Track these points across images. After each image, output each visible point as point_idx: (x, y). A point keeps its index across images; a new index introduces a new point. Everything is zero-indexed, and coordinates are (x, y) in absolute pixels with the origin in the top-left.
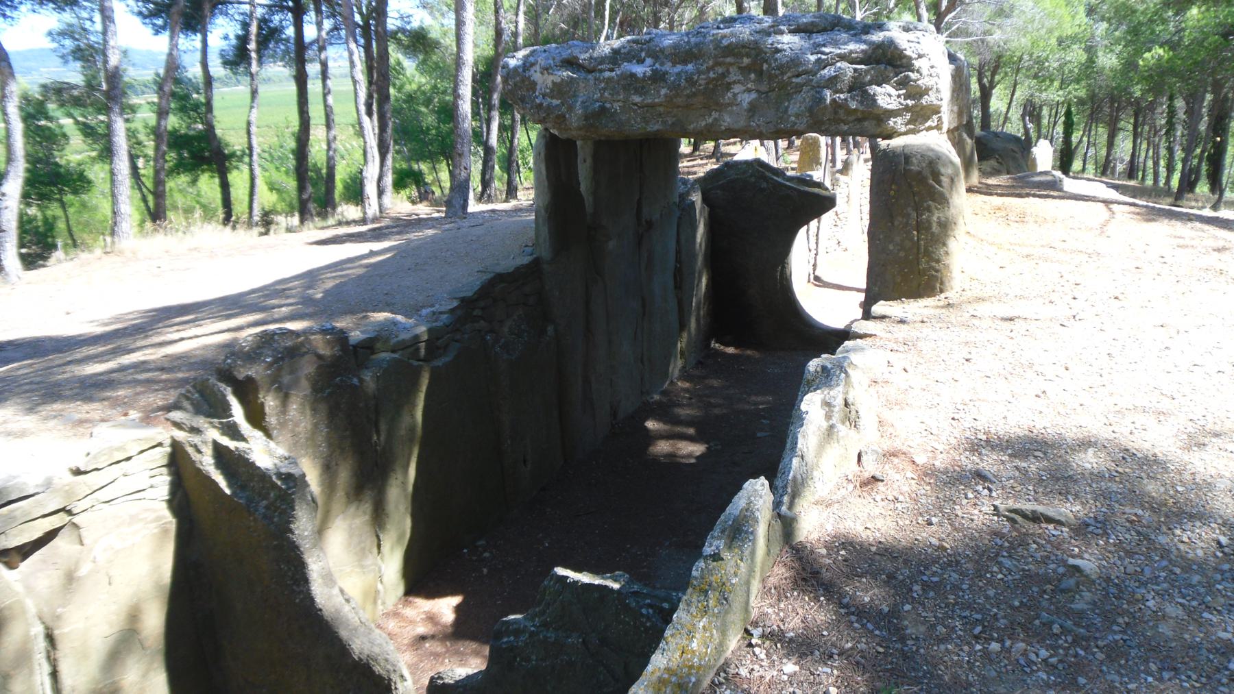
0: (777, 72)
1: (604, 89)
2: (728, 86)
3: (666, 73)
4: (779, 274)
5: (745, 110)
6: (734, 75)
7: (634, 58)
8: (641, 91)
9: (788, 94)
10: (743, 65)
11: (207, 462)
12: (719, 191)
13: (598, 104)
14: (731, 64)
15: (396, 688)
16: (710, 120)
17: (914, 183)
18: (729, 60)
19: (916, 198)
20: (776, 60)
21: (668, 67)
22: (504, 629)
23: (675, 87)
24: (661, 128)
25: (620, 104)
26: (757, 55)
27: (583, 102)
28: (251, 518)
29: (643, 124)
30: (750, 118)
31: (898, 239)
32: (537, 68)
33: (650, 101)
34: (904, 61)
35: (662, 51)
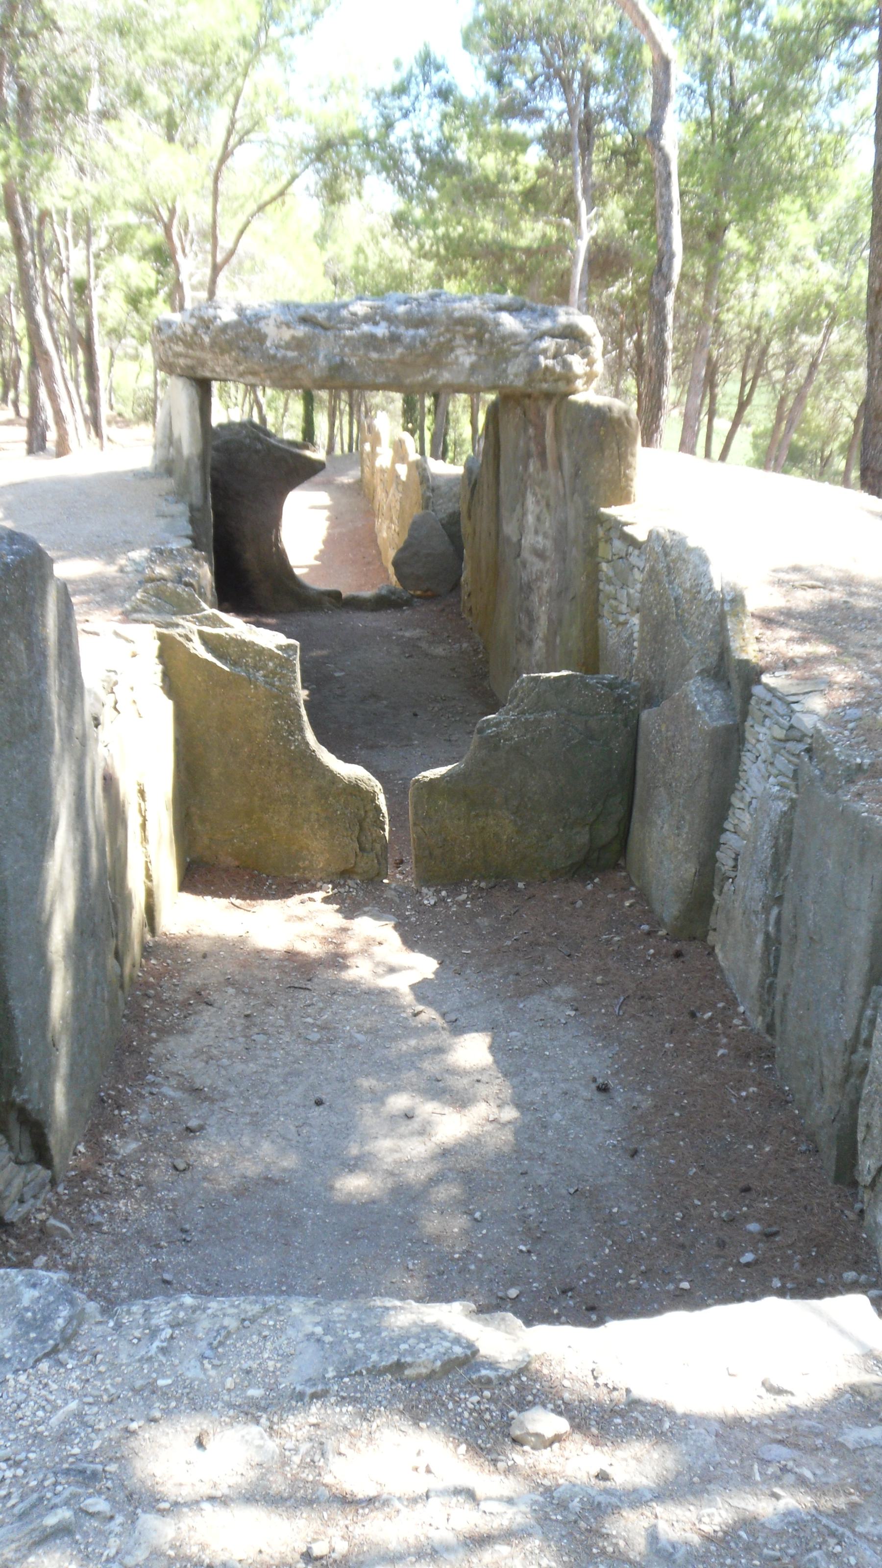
1: (344, 346)
2: (452, 350)
6: (459, 340)
11: (198, 649)
16: (428, 376)
18: (458, 328)
21: (402, 330)
23: (410, 348)
27: (326, 356)
31: (607, 465)
35: (396, 317)
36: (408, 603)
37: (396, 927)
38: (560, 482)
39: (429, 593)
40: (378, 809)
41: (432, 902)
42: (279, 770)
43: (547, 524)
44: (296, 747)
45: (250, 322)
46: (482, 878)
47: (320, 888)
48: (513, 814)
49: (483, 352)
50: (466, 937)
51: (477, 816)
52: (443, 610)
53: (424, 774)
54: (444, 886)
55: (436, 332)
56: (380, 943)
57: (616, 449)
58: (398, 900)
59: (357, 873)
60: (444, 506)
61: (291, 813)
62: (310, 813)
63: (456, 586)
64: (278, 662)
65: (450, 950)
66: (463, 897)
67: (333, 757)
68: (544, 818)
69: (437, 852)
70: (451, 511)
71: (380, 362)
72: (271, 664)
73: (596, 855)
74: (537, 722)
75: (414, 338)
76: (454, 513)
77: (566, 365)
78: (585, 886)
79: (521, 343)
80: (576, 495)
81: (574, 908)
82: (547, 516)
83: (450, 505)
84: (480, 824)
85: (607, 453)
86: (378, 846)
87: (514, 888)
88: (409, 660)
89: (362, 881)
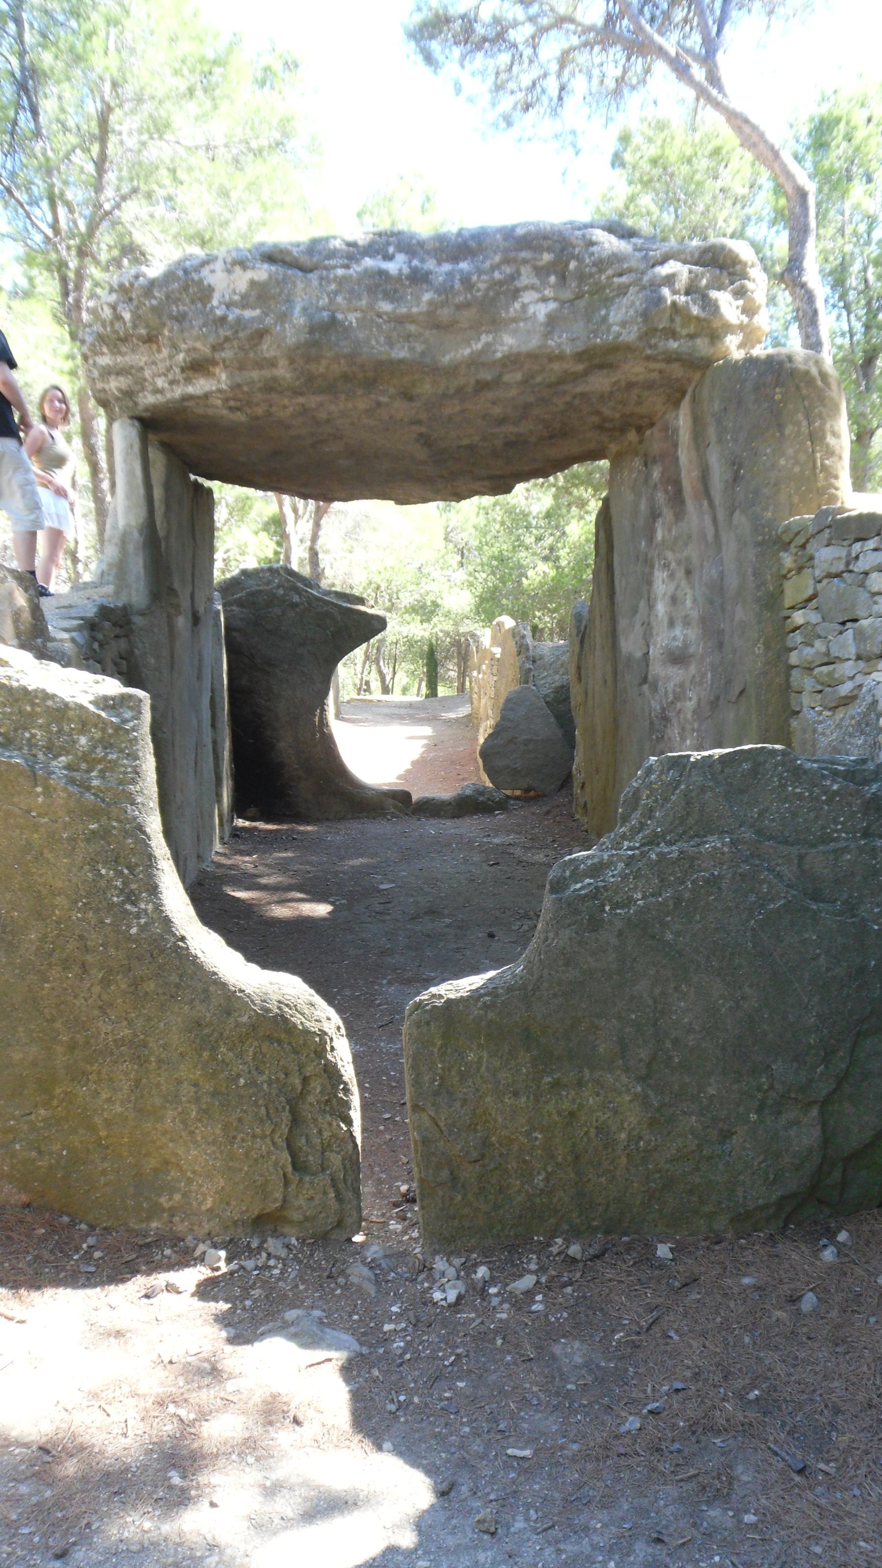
0: (594, 270)
1: (336, 293)
2: (516, 294)
3: (429, 273)
4: (317, 719)
5: (541, 324)
6: (527, 277)
7: (377, 252)
8: (392, 296)
9: (606, 299)
10: (541, 263)
12: (234, 608)
13: (325, 314)
14: (525, 261)
15: (333, 1049)
16: (479, 346)
17: (802, 384)
18: (524, 254)
19: (806, 403)
20: (593, 254)
21: (430, 264)
22: (568, 873)
23: (446, 290)
24: (408, 355)
25: (358, 315)
26: (563, 250)
27: (304, 309)
28: (39, 789)
29: (387, 348)
30: (548, 334)
31: (790, 452)
32: (219, 266)
33: (404, 310)
34: (738, 267)
36: (502, 805)
37: (348, 1371)
38: (708, 519)
39: (532, 793)
40: (332, 1073)
41: (452, 1296)
42: (105, 982)
43: (689, 603)
44: (143, 928)
45: (186, 272)
46: (574, 1234)
47: (201, 1260)
48: (642, 1079)
49: (567, 295)
50: (524, 1402)
51: (557, 1085)
52: (548, 813)
53: (433, 990)
54: (487, 1253)
55: (487, 264)
56: (296, 1421)
57: (805, 423)
58: (372, 1290)
59: (291, 1222)
60: (549, 680)
61: (138, 1082)
62: (179, 1082)
63: (567, 781)
64: (98, 735)
65: (477, 1447)
66: (527, 1282)
67: (237, 957)
68: (712, 1091)
69: (469, 1173)
70: (558, 684)
71: (399, 320)
72: (83, 740)
73: (837, 1175)
74: (688, 861)
75: (450, 275)
76: (562, 687)
77: (712, 307)
78: (816, 1253)
79: (630, 270)
80: (737, 514)
81: (799, 1312)
82: (689, 591)
83: (557, 677)
84: (566, 1105)
85: (789, 430)
86: (335, 1160)
87: (648, 1259)
88: (492, 869)
89: (302, 1241)
